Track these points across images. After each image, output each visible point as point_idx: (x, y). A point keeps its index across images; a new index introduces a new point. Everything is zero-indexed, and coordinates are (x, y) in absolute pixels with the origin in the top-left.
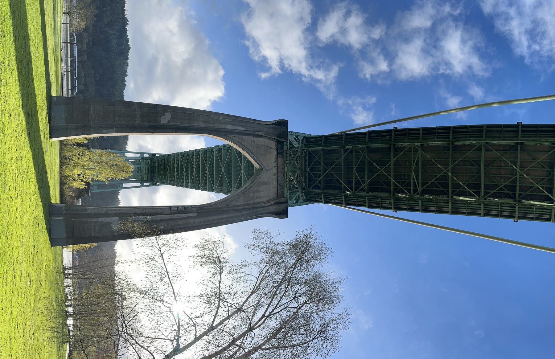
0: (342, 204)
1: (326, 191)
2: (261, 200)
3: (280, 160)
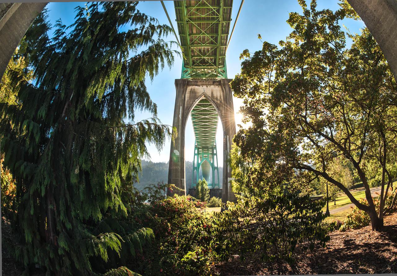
0: (225, 47)
1: (220, 32)
2: (222, 96)
3: (199, 83)
